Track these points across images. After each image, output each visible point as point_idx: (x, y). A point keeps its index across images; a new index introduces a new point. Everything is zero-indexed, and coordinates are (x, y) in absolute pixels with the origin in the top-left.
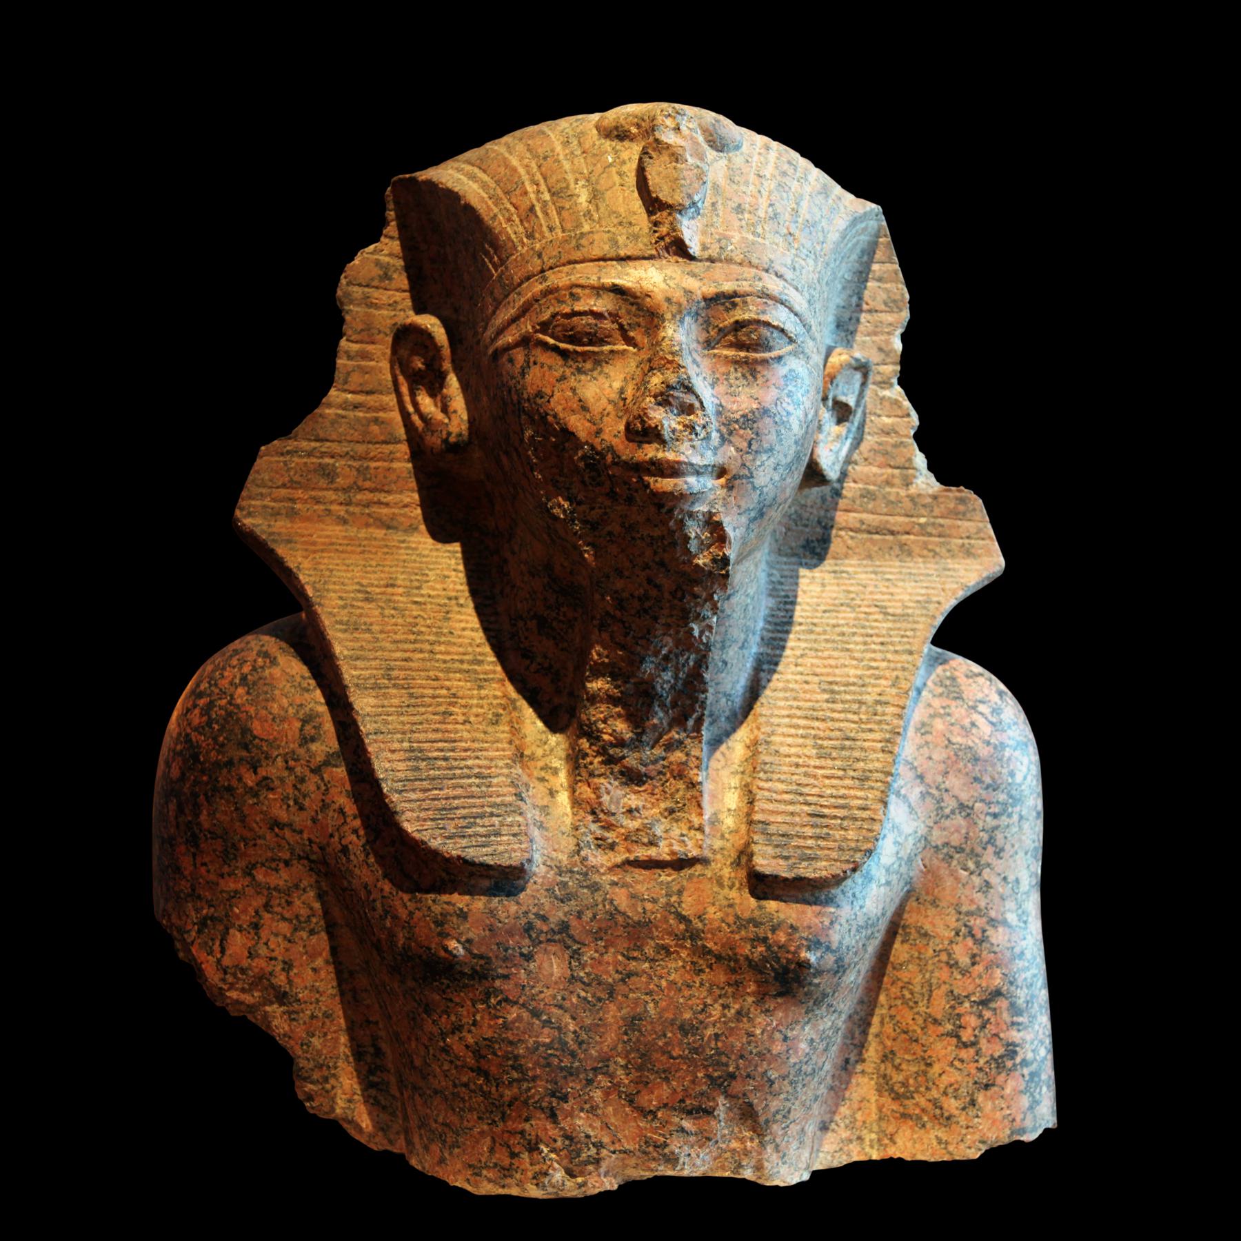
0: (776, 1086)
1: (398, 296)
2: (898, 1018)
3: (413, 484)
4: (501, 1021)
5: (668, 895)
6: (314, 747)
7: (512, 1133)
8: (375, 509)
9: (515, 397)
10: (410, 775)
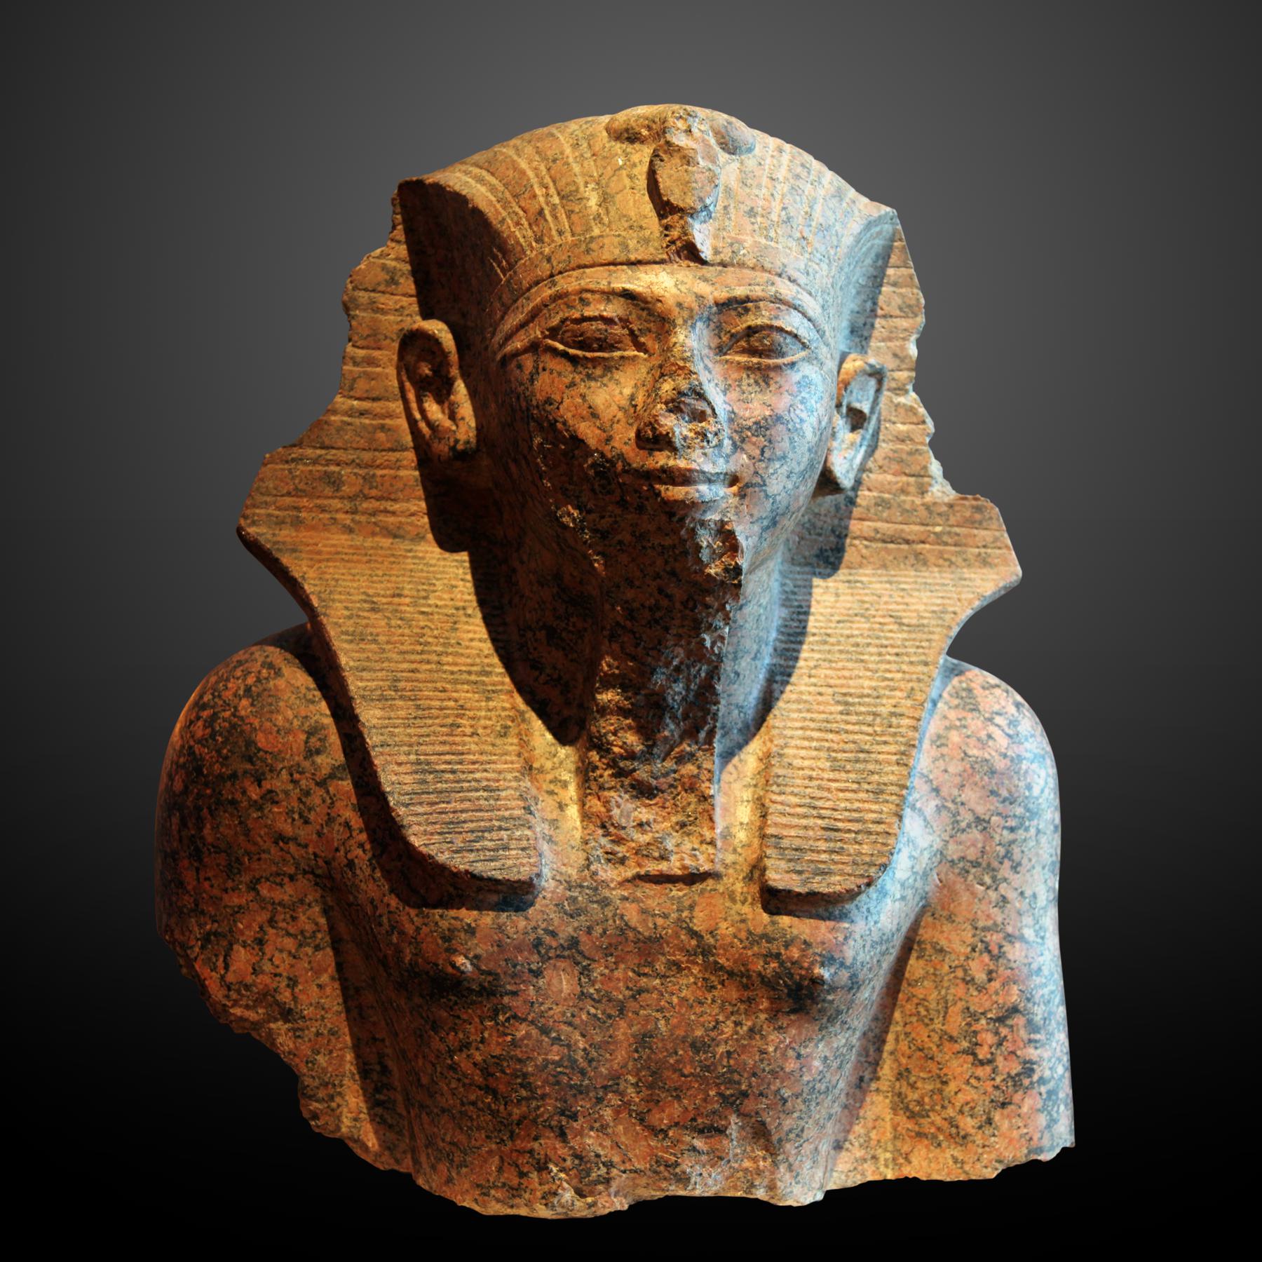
0: (789, 1104)
1: (405, 301)
2: (913, 1035)
3: (420, 492)
4: (509, 1038)
5: (680, 910)
6: (319, 760)
7: (521, 1152)
8: (381, 518)
9: (524, 404)
10: (417, 788)
